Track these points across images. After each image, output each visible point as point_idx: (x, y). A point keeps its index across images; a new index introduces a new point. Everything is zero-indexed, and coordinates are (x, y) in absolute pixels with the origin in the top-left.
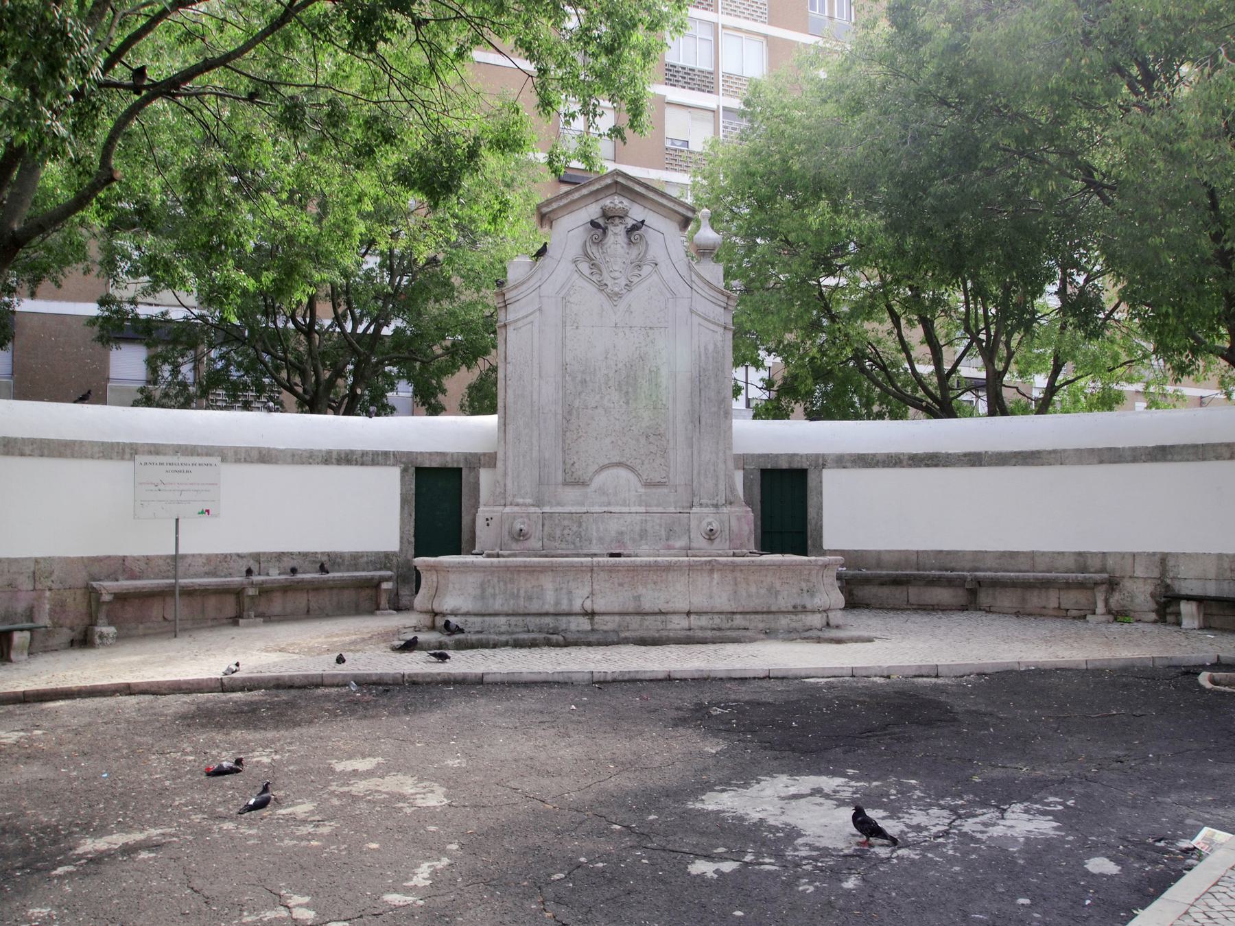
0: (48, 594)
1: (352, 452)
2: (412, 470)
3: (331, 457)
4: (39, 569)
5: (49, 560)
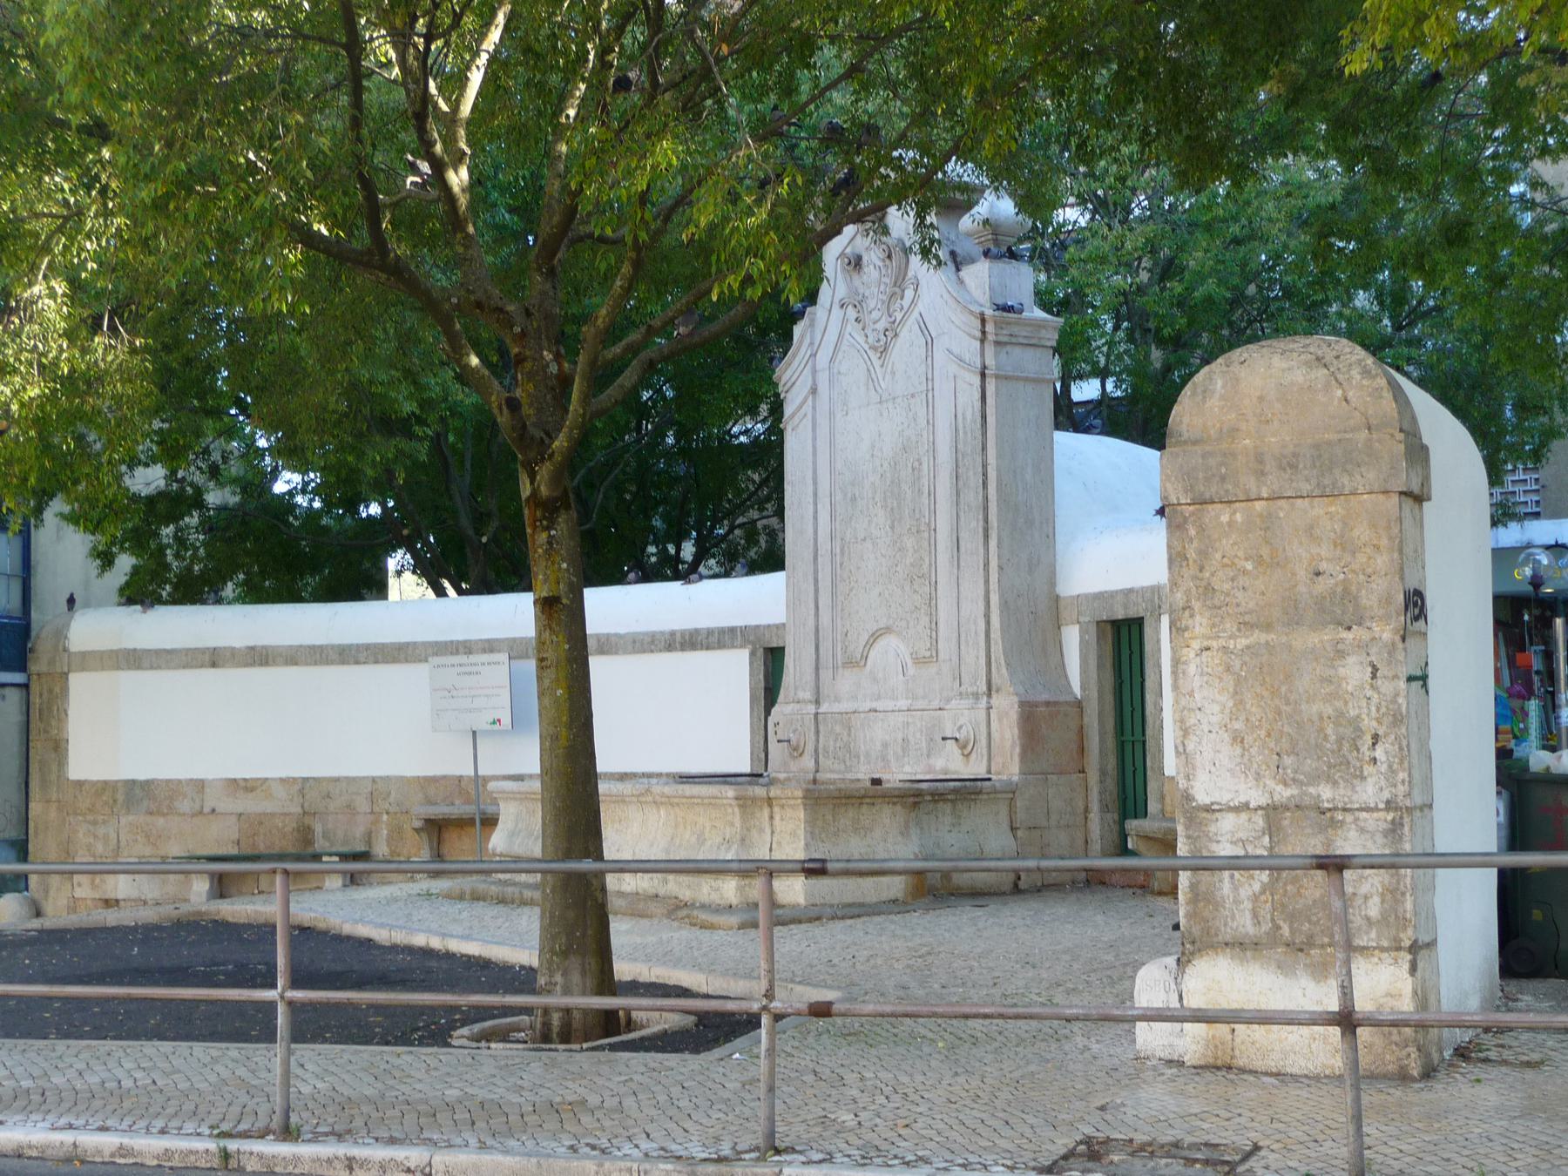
0: (385, 817)
1: (697, 631)
2: (760, 653)
3: (674, 641)
4: (377, 788)
5: (387, 779)
